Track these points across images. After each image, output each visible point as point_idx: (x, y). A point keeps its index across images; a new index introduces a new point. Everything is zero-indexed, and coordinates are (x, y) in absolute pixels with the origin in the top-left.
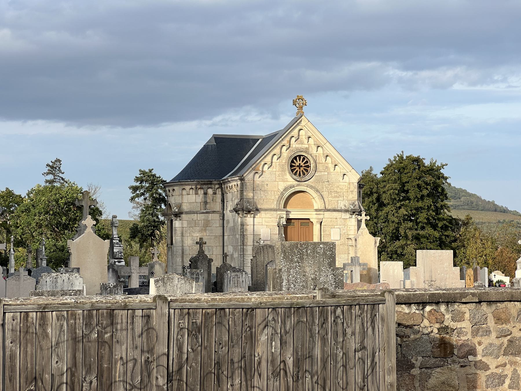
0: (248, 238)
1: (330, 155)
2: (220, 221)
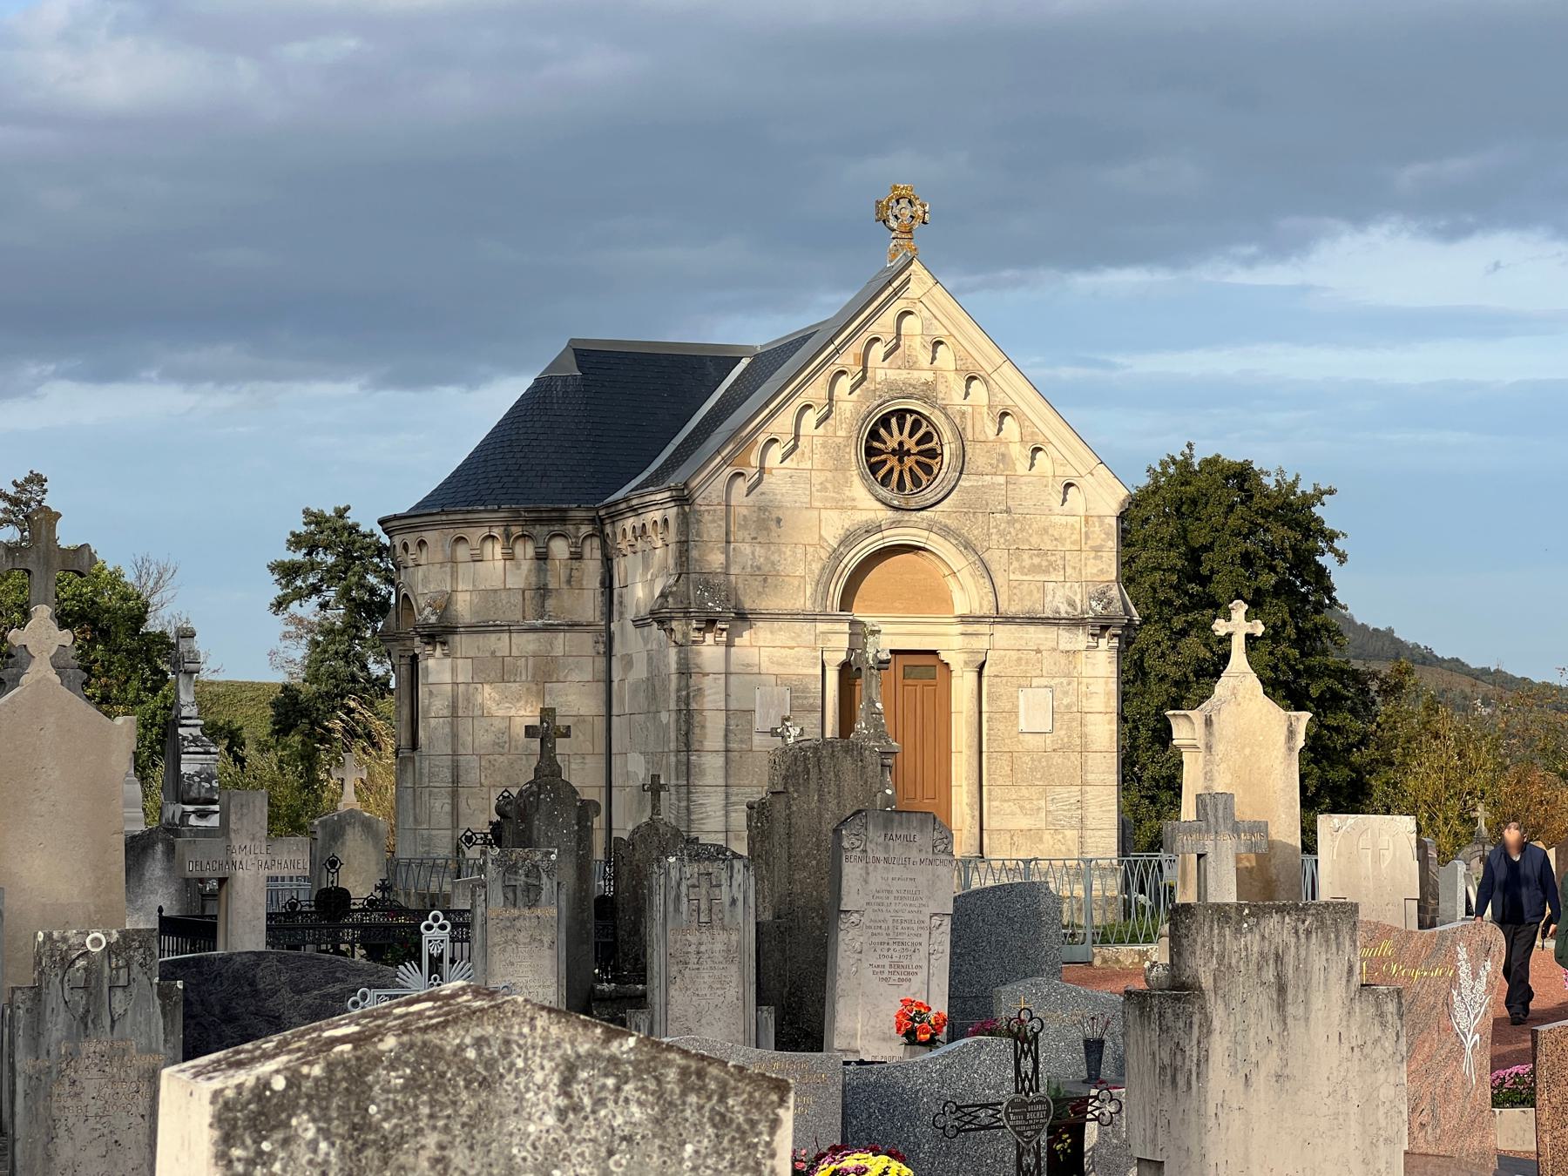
0: (708, 724)
1: (1016, 409)
2: (596, 659)
